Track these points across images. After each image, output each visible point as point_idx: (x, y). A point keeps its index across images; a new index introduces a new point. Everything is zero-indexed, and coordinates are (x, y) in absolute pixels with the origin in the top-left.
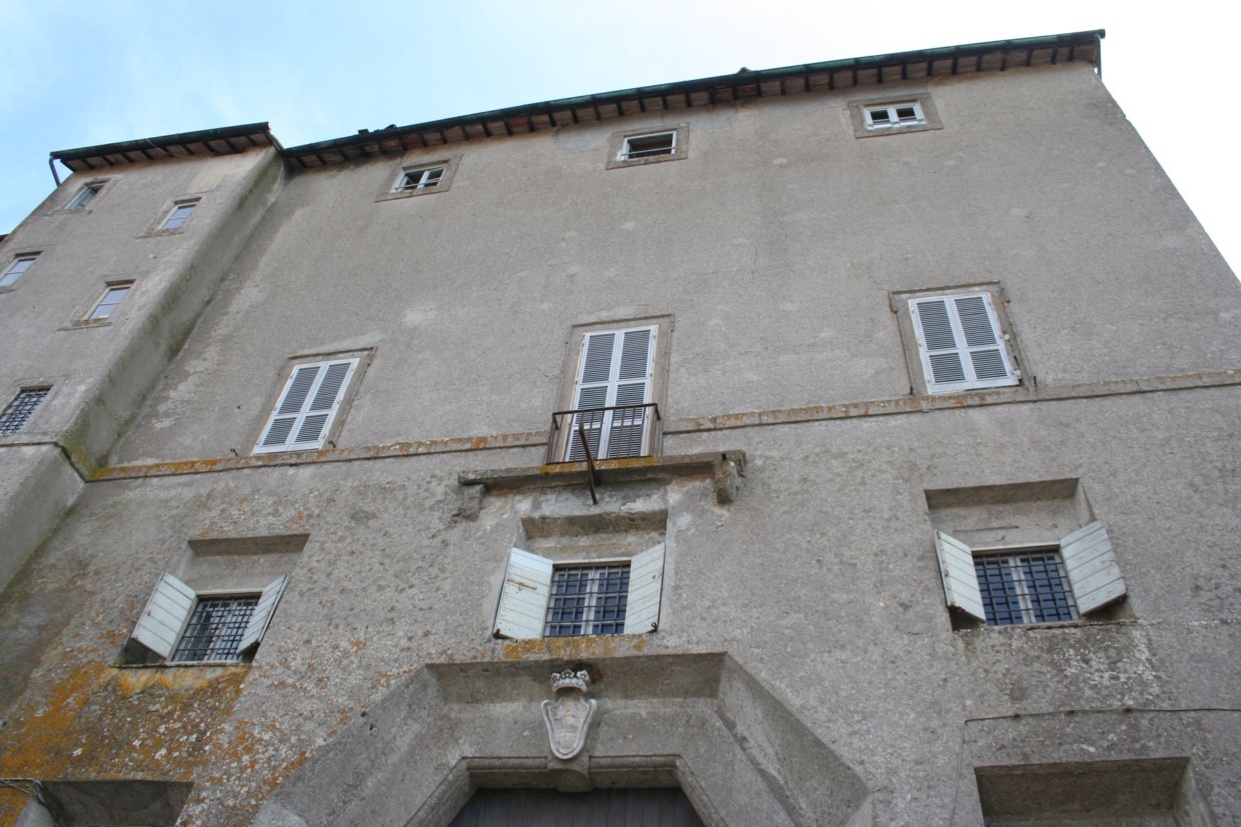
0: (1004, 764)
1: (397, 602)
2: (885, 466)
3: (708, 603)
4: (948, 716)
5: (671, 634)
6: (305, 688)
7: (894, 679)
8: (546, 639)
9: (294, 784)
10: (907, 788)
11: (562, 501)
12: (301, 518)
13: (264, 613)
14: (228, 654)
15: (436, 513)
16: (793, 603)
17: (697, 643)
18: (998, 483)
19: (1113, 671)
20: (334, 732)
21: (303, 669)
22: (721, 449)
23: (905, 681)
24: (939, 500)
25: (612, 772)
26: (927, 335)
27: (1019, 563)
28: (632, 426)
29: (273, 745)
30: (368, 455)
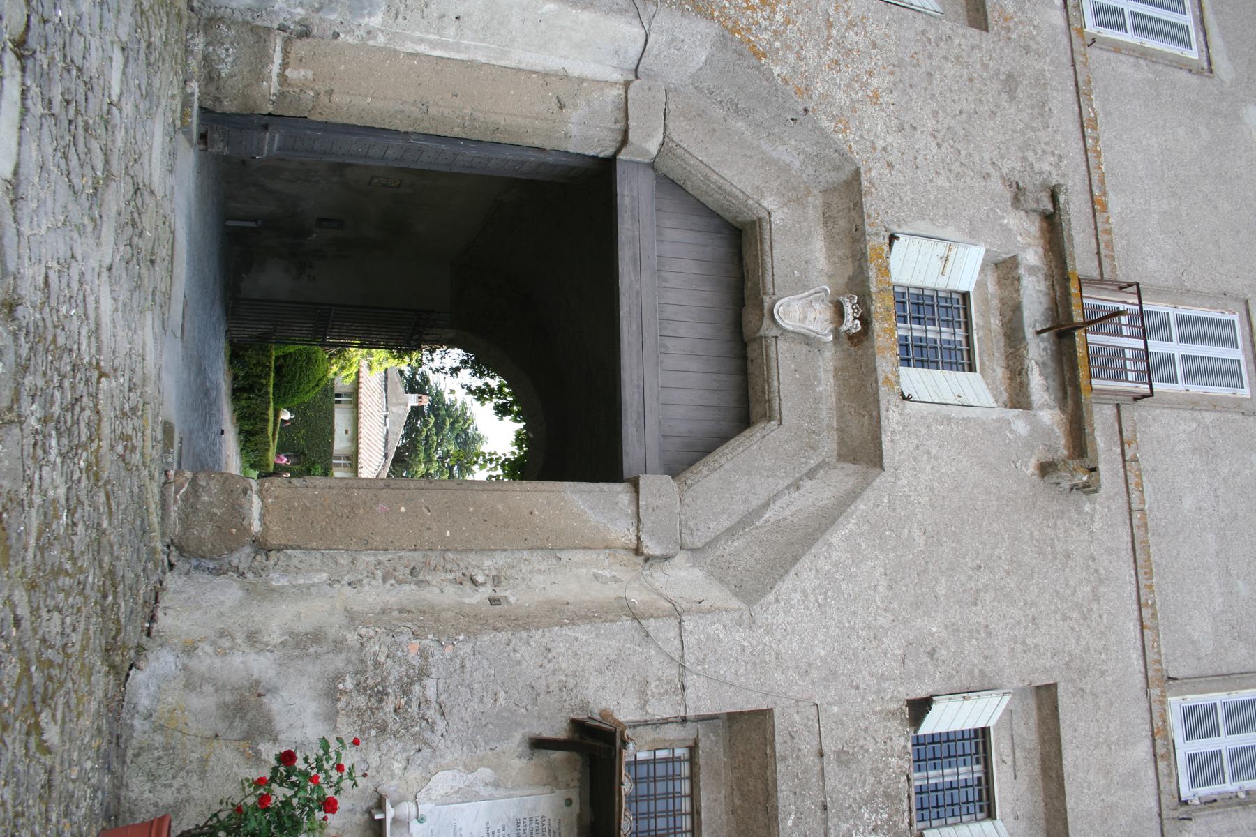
2: (1084, 643)
3: (934, 451)
4: (822, 687)
5: (901, 415)
7: (859, 637)
8: (891, 288)
9: (735, 51)
11: (1038, 297)
12: (1006, 20)
15: (1020, 164)
17: (892, 441)
18: (1064, 762)
20: (787, 83)
21: (847, 44)
22: (1101, 467)
23: (857, 648)
24: (1046, 697)
26: (1243, 702)
27: (976, 775)
28: (1126, 370)
29: (771, 25)
30: (1080, 84)
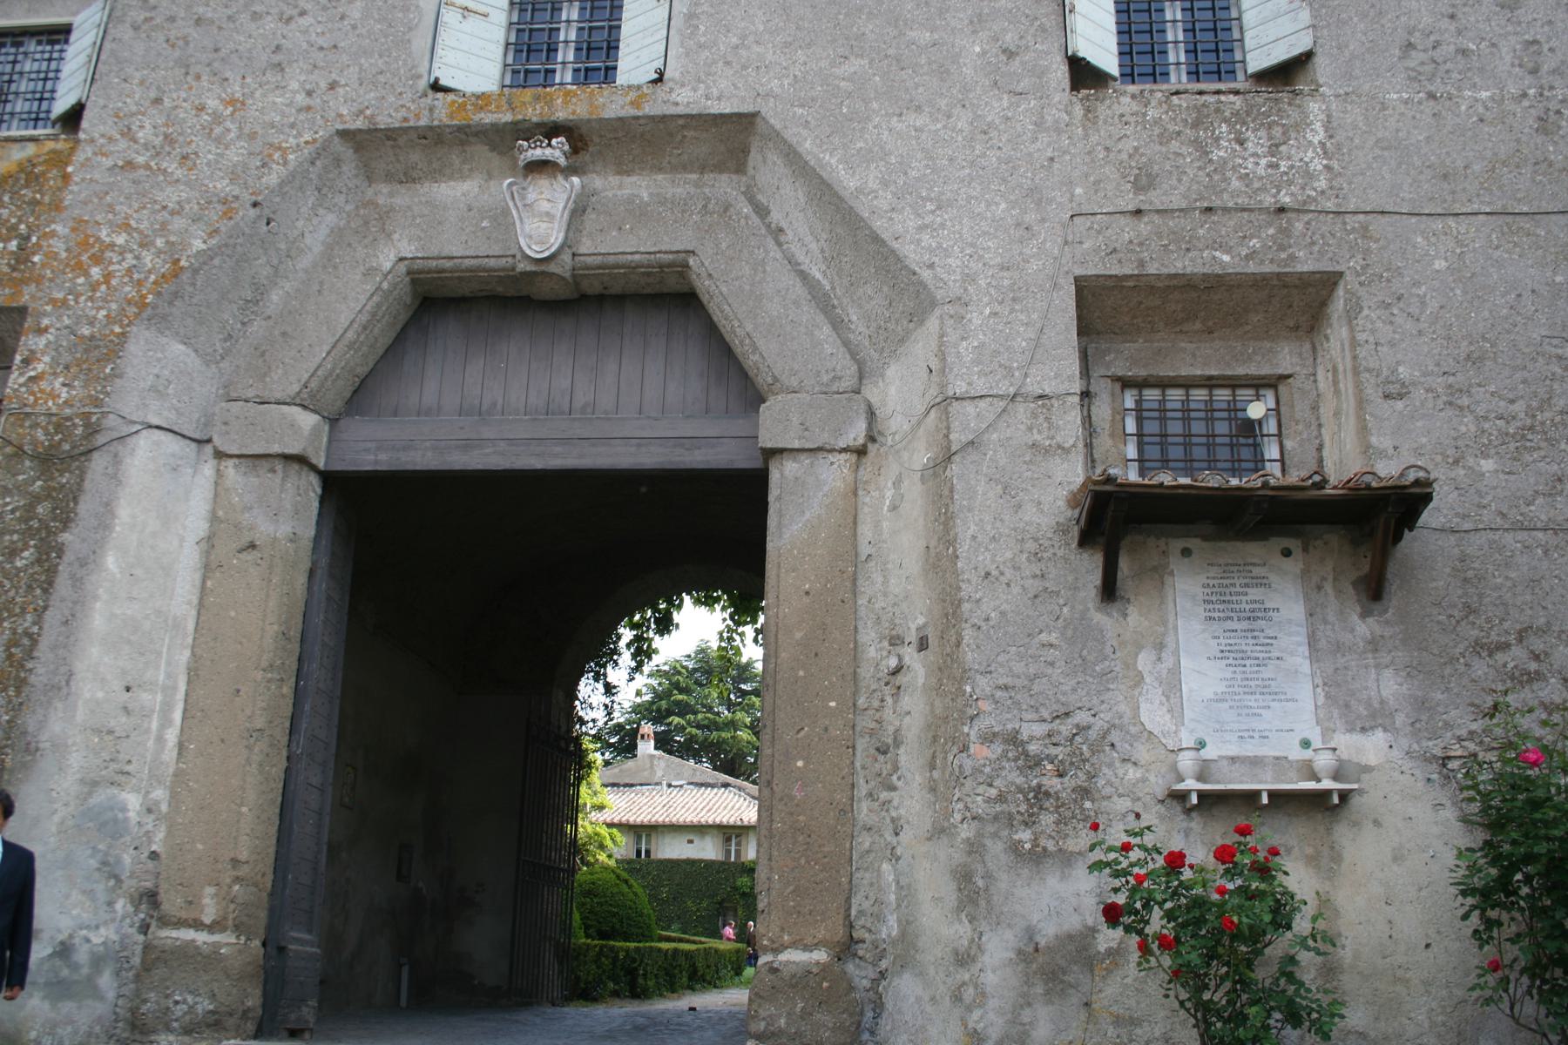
0: (1113, 273)
1: (284, 37)
3: (735, 40)
4: (1049, 208)
5: (683, 85)
6: (165, 170)
7: (983, 155)
9: (171, 303)
10: (985, 300)
13: (82, 58)
14: (37, 120)
16: (853, 42)
17: (719, 99)
19: (1273, 156)
20: (216, 231)
23: (999, 158)
25: (603, 274)
29: (131, 251)
